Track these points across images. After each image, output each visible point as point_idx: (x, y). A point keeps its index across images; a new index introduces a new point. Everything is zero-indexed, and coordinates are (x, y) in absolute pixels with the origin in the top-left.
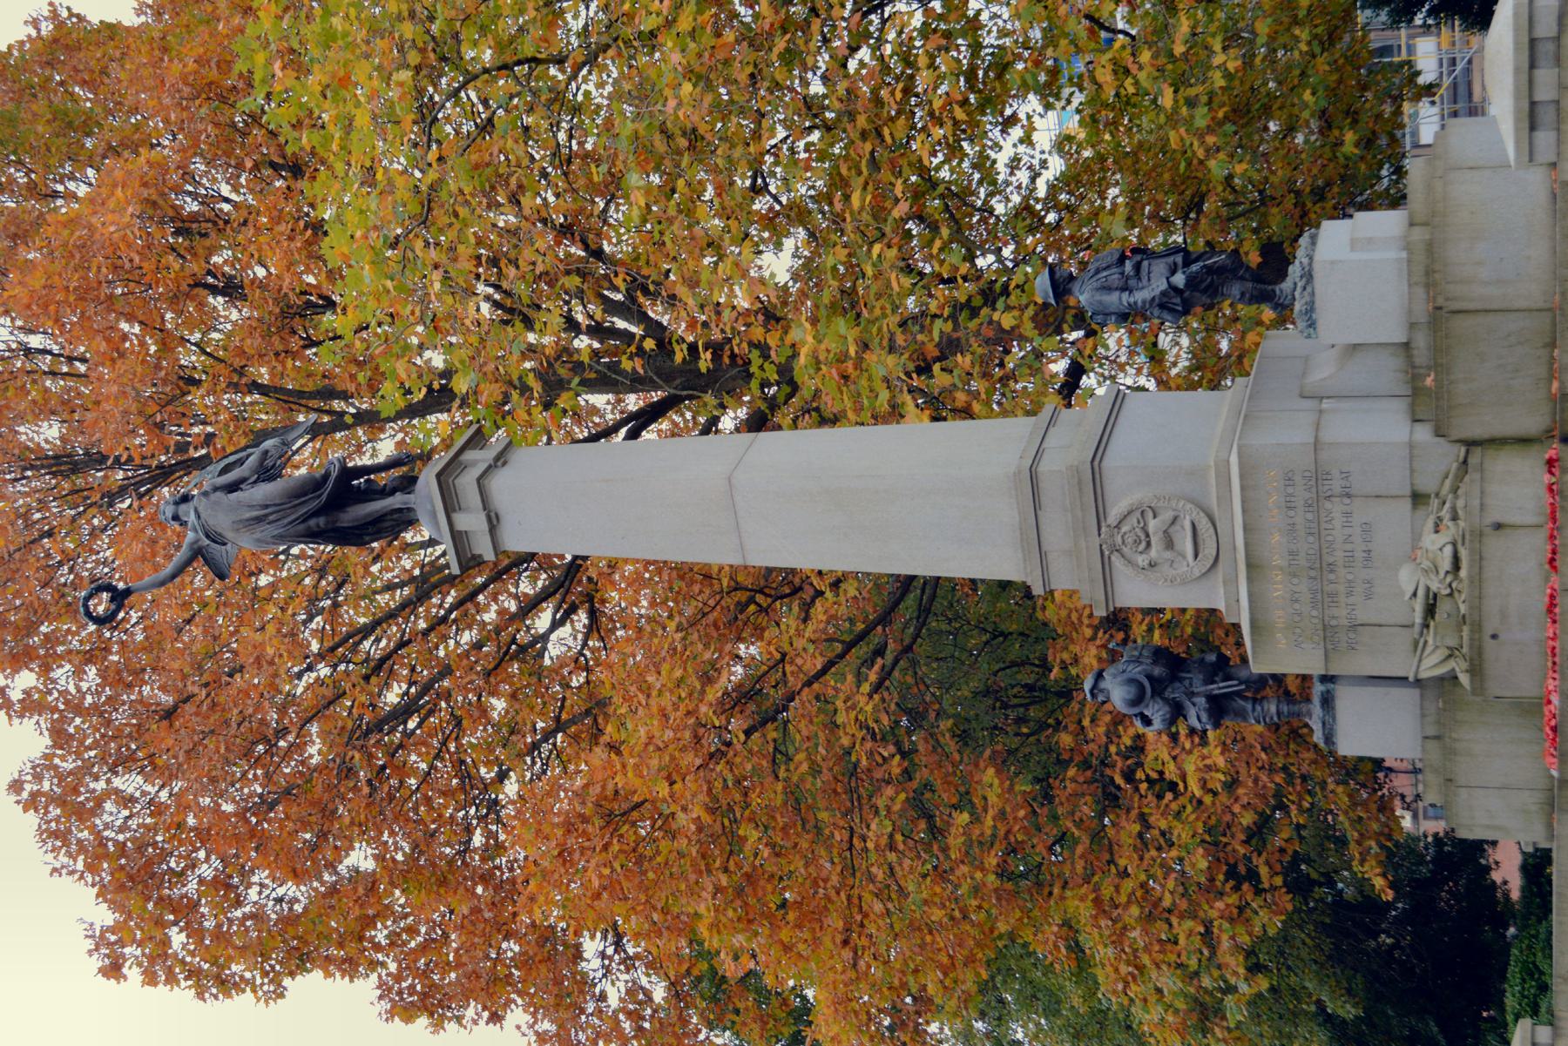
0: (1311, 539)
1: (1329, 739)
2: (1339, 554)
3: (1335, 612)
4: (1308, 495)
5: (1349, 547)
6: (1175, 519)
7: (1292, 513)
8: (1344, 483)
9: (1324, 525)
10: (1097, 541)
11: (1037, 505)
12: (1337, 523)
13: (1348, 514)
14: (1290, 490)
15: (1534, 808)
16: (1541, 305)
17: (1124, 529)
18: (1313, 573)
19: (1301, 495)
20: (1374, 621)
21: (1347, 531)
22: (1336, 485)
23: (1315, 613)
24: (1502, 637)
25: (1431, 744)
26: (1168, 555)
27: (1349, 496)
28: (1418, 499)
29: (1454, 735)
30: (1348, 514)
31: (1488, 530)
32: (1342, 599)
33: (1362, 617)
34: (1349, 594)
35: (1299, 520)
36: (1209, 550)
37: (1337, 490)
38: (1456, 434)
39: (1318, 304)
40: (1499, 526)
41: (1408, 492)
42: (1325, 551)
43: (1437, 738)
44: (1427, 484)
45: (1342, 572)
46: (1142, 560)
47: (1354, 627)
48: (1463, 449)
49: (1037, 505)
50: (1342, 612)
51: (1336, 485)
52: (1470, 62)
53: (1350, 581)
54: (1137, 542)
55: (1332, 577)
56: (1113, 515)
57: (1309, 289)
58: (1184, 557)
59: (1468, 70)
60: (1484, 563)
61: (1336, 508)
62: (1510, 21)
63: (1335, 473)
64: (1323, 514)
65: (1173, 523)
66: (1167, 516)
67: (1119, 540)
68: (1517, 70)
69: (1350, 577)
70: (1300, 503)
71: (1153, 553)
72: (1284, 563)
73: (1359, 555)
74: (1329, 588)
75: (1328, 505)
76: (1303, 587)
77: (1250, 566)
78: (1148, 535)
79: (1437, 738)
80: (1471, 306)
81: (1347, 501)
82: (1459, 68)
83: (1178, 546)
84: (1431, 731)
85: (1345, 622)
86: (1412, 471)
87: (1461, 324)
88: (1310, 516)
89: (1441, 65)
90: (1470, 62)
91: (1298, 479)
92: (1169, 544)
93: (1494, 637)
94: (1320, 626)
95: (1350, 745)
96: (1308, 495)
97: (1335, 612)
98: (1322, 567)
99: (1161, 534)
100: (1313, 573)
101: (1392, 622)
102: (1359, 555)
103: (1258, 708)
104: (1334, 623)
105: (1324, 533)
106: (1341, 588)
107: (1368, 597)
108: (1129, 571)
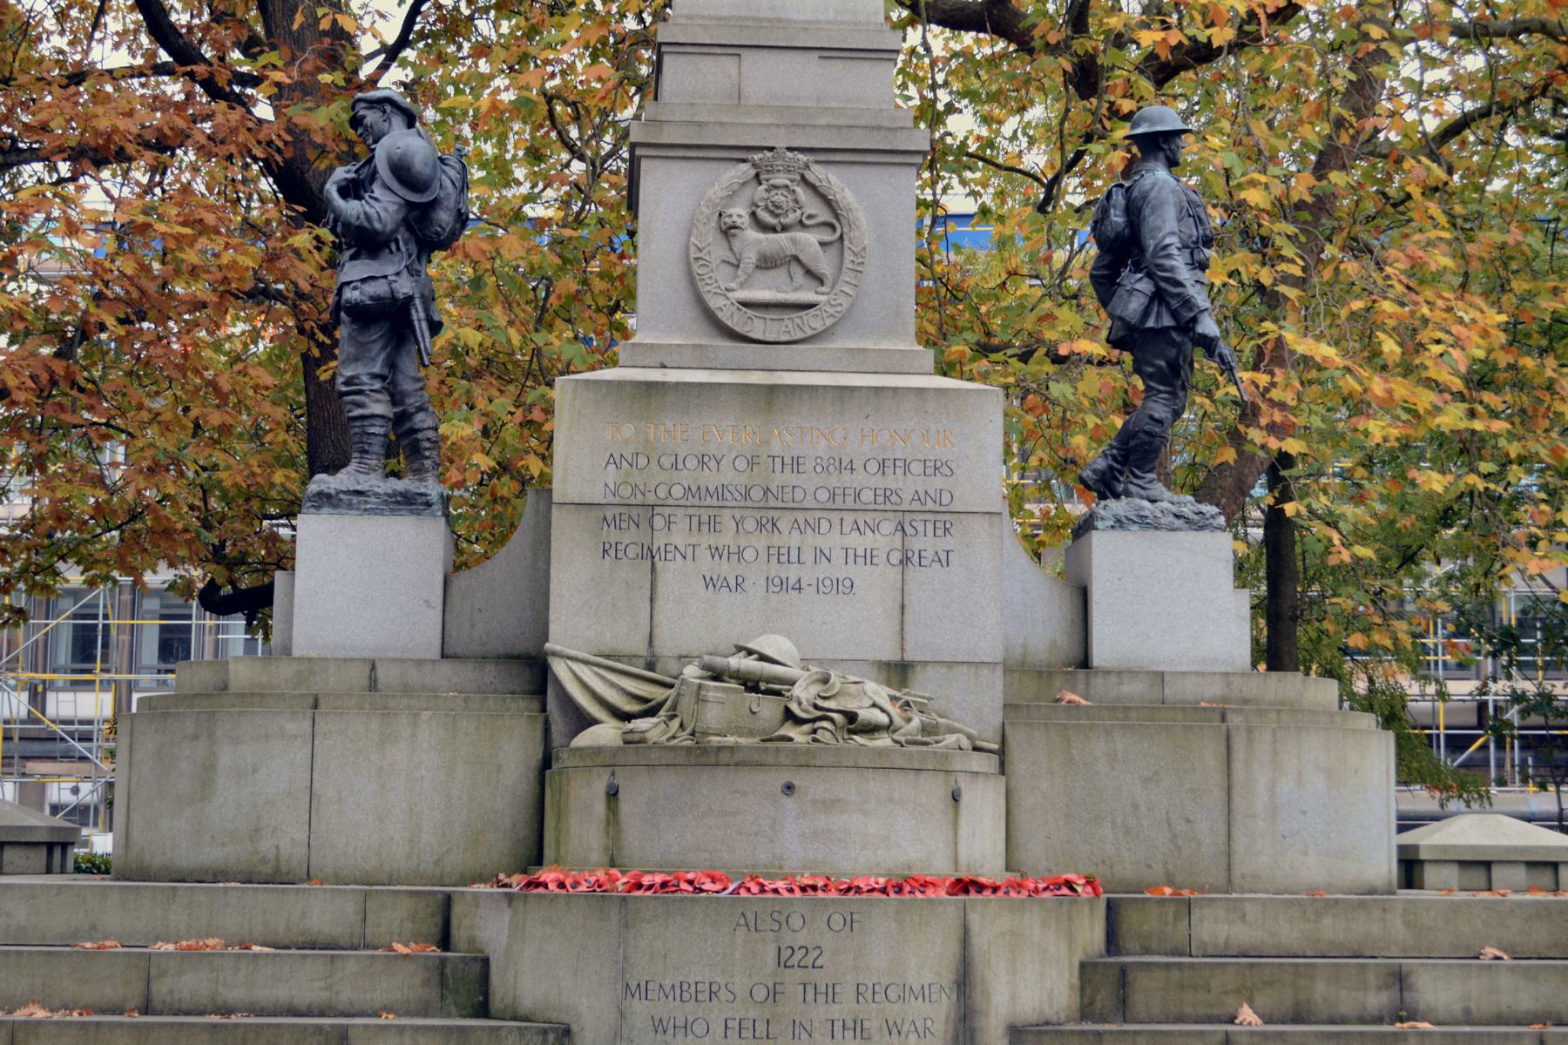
0: (823, 496)
1: (325, 500)
2: (794, 540)
3: (680, 525)
4: (907, 496)
5: (808, 556)
6: (819, 279)
7: (873, 467)
8: (929, 554)
9: (849, 518)
10: (780, 144)
11: (828, 52)
12: (853, 540)
13: (869, 557)
14: (916, 468)
15: (266, 846)
16: (1238, 870)
17: (800, 191)
18: (757, 494)
19: (908, 486)
20: (661, 588)
21: (838, 556)
22: (923, 543)
23: (677, 492)
24: (789, 802)
25: (360, 675)
26: (750, 258)
27: (905, 561)
28: (899, 672)
29: (425, 715)
30: (869, 557)
31: (953, 786)
32: (707, 539)
33: (670, 572)
34: (715, 552)
35: (858, 479)
36: (757, 327)
37: (916, 544)
38: (1016, 738)
39: (1151, 534)
40: (956, 798)
41: (909, 657)
42: (801, 516)
43: (373, 685)
44: (923, 686)
45: (761, 542)
46: (739, 213)
47: (650, 555)
48: (995, 747)
49: (828, 52)
50: (679, 537)
51: (923, 543)
52: (83, 759)
53: (740, 553)
54: (775, 210)
55: (750, 525)
56: (831, 178)
57: (1179, 523)
58: (742, 286)
59: (68, 756)
60: (911, 775)
61: (884, 539)
62: (1544, 843)
63: (948, 543)
64: (869, 517)
65: (809, 273)
66: (824, 264)
67: (780, 180)
68: (1526, 849)
69: (749, 555)
70: (891, 481)
71: (753, 234)
72: (776, 449)
73: (793, 573)
74: (727, 519)
75: (887, 527)
76: (729, 476)
77: (772, 389)
78: (785, 228)
79: (373, 685)
80: (1238, 766)
81: (896, 557)
82: (78, 745)
83: (762, 276)
84: (385, 675)
85: (660, 541)
86: (950, 664)
87: (1209, 754)
88: (867, 496)
89: (81, 722)
90: (83, 759)
91: (938, 482)
92: (767, 263)
93: (789, 788)
94: (651, 499)
95: (317, 539)
96: (907, 496)
97: (680, 525)
98: (769, 509)
99: (791, 250)
100: (757, 494)
101: (658, 618)
102: (793, 573)
103: (377, 385)
104: (659, 522)
105: (835, 517)
106: (727, 539)
107: (709, 583)
108: (716, 192)
